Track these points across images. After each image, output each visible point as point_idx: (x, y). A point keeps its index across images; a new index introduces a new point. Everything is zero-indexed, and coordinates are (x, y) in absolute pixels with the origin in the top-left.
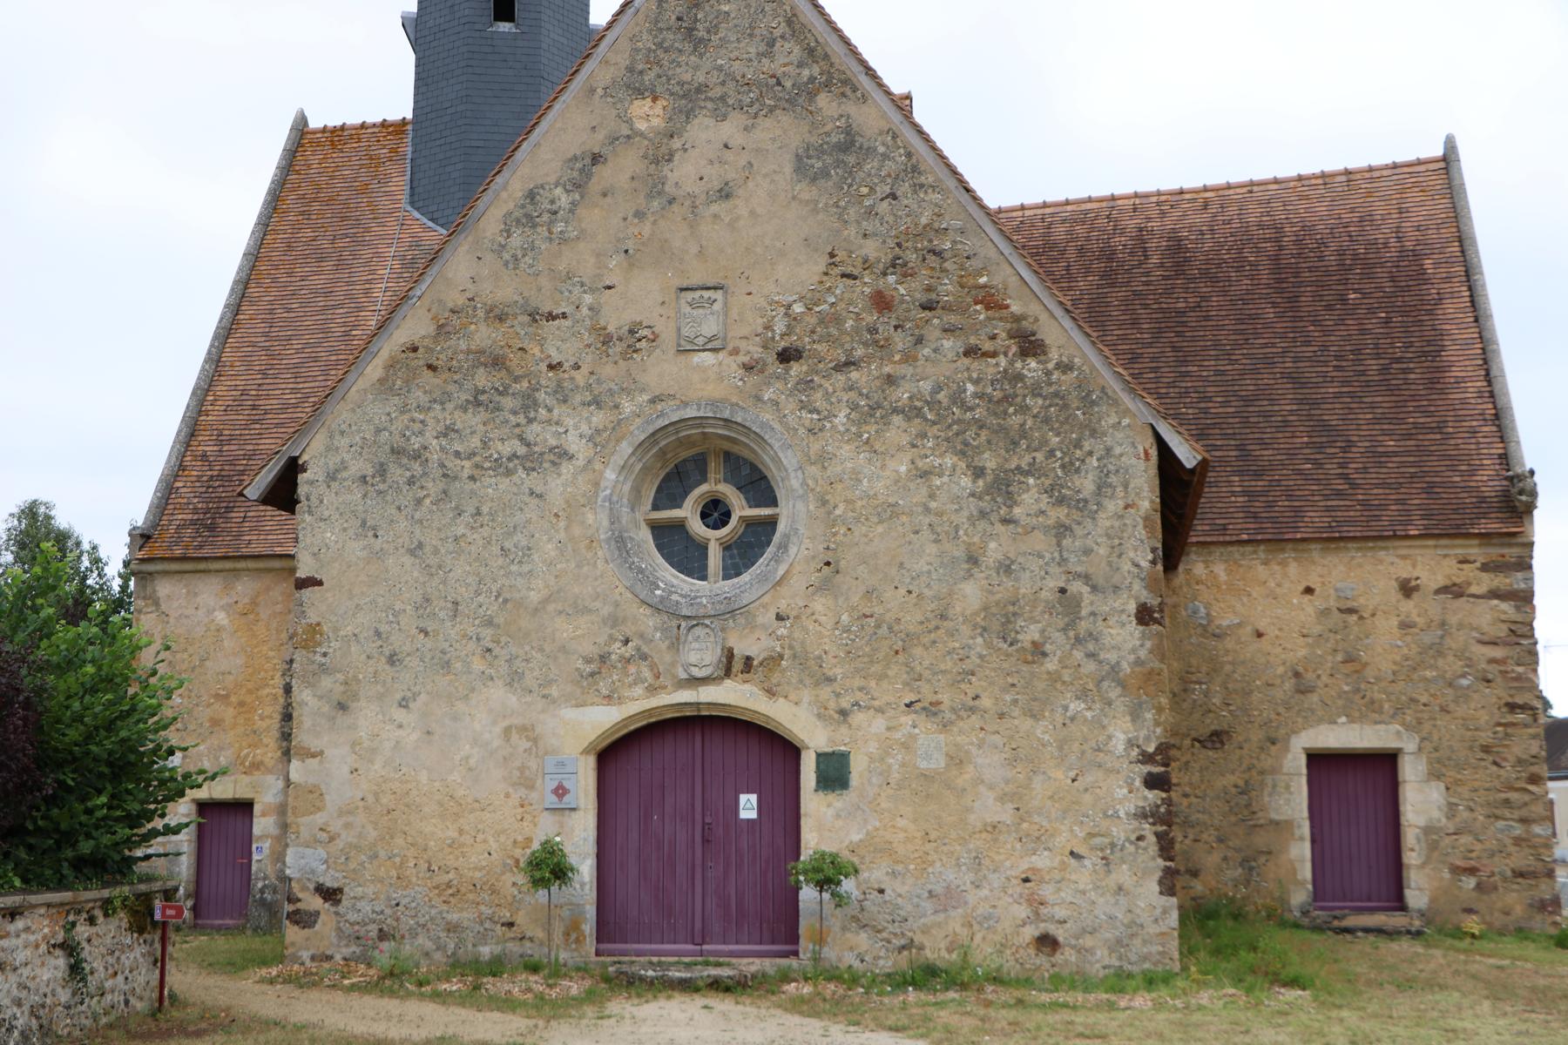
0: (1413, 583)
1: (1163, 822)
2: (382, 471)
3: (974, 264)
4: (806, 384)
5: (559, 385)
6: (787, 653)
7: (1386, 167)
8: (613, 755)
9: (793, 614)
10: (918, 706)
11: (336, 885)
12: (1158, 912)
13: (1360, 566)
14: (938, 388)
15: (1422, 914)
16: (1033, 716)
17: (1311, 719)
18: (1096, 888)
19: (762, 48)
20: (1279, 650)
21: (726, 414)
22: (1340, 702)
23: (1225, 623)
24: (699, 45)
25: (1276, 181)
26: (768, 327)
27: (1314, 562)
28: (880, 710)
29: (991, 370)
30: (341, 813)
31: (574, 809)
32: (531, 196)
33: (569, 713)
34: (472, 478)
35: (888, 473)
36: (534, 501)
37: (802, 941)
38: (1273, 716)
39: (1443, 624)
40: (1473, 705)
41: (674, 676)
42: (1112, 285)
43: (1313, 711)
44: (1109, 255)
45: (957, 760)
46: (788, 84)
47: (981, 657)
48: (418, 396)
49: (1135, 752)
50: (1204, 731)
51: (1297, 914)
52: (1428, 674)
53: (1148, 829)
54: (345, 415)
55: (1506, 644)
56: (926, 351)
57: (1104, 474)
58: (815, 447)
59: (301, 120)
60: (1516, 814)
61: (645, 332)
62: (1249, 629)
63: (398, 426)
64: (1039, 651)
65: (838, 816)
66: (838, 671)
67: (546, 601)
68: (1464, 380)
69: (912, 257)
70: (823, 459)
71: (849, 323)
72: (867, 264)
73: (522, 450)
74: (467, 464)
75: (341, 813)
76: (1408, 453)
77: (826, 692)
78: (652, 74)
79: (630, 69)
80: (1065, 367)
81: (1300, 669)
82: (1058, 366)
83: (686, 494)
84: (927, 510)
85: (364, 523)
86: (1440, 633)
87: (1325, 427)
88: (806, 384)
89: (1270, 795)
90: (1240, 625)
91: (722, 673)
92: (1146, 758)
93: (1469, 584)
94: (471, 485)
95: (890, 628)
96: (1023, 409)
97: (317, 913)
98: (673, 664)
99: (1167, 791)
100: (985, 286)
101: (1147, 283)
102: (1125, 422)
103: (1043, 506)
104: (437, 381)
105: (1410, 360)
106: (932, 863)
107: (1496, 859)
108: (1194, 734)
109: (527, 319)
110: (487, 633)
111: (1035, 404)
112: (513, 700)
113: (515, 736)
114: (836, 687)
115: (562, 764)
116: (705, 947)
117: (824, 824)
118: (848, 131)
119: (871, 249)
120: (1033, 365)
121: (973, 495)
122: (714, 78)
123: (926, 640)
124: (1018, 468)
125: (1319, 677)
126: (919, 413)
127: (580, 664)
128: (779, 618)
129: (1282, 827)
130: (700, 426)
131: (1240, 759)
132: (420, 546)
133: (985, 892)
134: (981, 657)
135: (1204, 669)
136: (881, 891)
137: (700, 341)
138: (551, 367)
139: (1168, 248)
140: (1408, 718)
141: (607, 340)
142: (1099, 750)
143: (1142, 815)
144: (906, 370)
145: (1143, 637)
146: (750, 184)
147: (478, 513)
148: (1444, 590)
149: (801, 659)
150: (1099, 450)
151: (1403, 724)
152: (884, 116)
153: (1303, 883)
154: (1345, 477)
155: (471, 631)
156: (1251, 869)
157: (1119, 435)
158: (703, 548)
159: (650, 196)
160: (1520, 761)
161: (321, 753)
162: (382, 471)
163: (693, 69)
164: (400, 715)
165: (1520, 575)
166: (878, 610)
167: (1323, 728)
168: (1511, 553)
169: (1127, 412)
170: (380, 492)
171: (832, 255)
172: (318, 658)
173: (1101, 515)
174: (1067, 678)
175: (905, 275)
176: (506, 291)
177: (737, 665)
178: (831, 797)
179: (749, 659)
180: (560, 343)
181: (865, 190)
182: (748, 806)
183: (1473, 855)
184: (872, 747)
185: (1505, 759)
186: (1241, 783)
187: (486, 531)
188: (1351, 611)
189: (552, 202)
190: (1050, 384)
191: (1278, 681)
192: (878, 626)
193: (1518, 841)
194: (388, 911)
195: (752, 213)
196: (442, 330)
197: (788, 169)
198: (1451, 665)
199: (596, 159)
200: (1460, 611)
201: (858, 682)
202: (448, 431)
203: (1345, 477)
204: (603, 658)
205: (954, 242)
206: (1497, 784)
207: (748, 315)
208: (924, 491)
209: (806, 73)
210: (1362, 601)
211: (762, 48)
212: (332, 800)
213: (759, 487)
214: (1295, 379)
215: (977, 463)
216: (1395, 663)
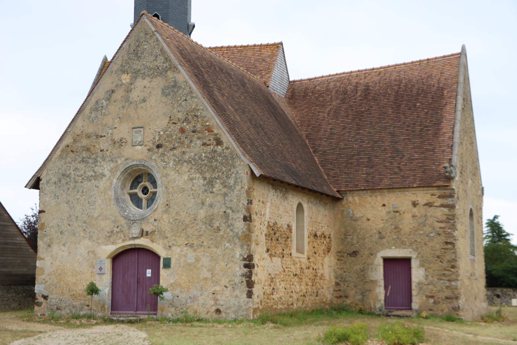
0: (417, 202)
1: (248, 278)
2: (60, 181)
3: (206, 119)
4: (163, 154)
5: (103, 156)
6: (157, 230)
7: (441, 57)
8: (117, 258)
9: (158, 219)
10: (188, 245)
12: (246, 303)
13: (400, 197)
14: (195, 155)
15: (416, 311)
16: (217, 247)
17: (383, 247)
18: (231, 296)
19: (154, 58)
20: (374, 225)
21: (143, 163)
22: (393, 242)
23: (358, 216)
24: (139, 58)
25: (404, 64)
26: (154, 138)
27: (385, 196)
28: (179, 246)
29: (209, 149)
30: (48, 275)
31: (104, 274)
32: (97, 102)
33: (103, 247)
34: (81, 182)
35: (182, 179)
36: (96, 188)
37: (158, 311)
38: (372, 246)
39: (426, 216)
40: (434, 243)
41: (129, 237)
42: (344, 103)
43: (384, 245)
44: (345, 92)
45: (197, 260)
46: (160, 68)
47: (204, 231)
48: (69, 159)
49: (242, 258)
50: (351, 251)
51: (378, 310)
52: (421, 232)
53: (244, 279)
54: (51, 165)
55: (445, 222)
56: (193, 144)
57: (236, 178)
58: (165, 172)
60: (447, 278)
61: (124, 140)
62: (365, 218)
63: (64, 168)
64: (218, 229)
65: (168, 276)
66: (169, 235)
67: (99, 216)
68: (446, 133)
69: (190, 117)
70: (167, 176)
71: (174, 137)
72: (179, 120)
73: (93, 174)
74: (80, 178)
75: (48, 275)
76: (421, 159)
77: (166, 241)
78: (127, 67)
79: (122, 65)
80: (227, 148)
81: (381, 231)
82: (226, 148)
84: (192, 189)
85: (55, 195)
86: (424, 219)
87: (397, 151)
88: (163, 154)
89: (371, 272)
90: (363, 217)
91: (140, 236)
92: (244, 259)
93: (434, 202)
94: (81, 184)
95: (182, 223)
96: (217, 160)
97: (42, 303)
98: (129, 233)
99: (250, 268)
100: (208, 125)
101: (354, 102)
102: (242, 164)
103: (221, 188)
104: (73, 155)
105: (430, 126)
106: (191, 289)
107: (440, 293)
108: (348, 252)
109: (95, 137)
110: (84, 225)
111: (219, 159)
112: (90, 244)
114: (168, 239)
115: (101, 261)
116: (137, 312)
117: (166, 278)
118: (175, 82)
119: (180, 115)
120: (220, 148)
121: (203, 185)
122: (142, 68)
123: (191, 226)
124: (215, 177)
125: (386, 233)
126: (190, 162)
127: (106, 233)
128: (155, 220)
130: (137, 166)
131: (362, 260)
132: (69, 201)
133: (203, 297)
134: (204, 231)
135: (351, 231)
137: (137, 143)
138: (101, 151)
139: (364, 89)
140: (414, 247)
142: (233, 257)
143: (243, 275)
144: (188, 150)
145: (244, 225)
146: (151, 98)
147: (83, 192)
148: (426, 204)
149: (160, 232)
150: (235, 172)
151: (412, 249)
152: (184, 77)
153: (380, 300)
154: (399, 167)
155: (80, 224)
156: (364, 296)
157: (240, 168)
158: (141, 200)
159: (126, 102)
160: (449, 261)
161: (44, 259)
162: (60, 181)
163: (137, 65)
164: (63, 248)
165: (450, 199)
166: (179, 218)
167: (387, 250)
168: (448, 192)
169: (242, 161)
170: (59, 186)
171: (170, 117)
172: (44, 232)
173: (235, 190)
174: (225, 237)
175: (188, 123)
176: (90, 129)
177: (144, 234)
179: (147, 232)
180: (104, 144)
181: (179, 99)
182: (149, 273)
183: (433, 292)
184: (177, 256)
185: (444, 260)
186: (362, 268)
187: (84, 197)
188: (397, 212)
189: (102, 104)
190: (223, 153)
191: (374, 235)
192: (179, 222)
193: (447, 287)
194: (59, 302)
195: (151, 106)
196: (75, 141)
197: (160, 93)
198: (428, 229)
199: (113, 91)
200: (431, 211)
201: (174, 238)
202: (76, 169)
203: (399, 167)
204: (112, 232)
205: (201, 113)
206: (441, 268)
207: (150, 135)
208: (191, 184)
209: (165, 65)
210: (400, 208)
211: (154, 58)
212: (47, 272)
213: (154, 183)
214: (392, 134)
215: (205, 176)
216: (410, 229)
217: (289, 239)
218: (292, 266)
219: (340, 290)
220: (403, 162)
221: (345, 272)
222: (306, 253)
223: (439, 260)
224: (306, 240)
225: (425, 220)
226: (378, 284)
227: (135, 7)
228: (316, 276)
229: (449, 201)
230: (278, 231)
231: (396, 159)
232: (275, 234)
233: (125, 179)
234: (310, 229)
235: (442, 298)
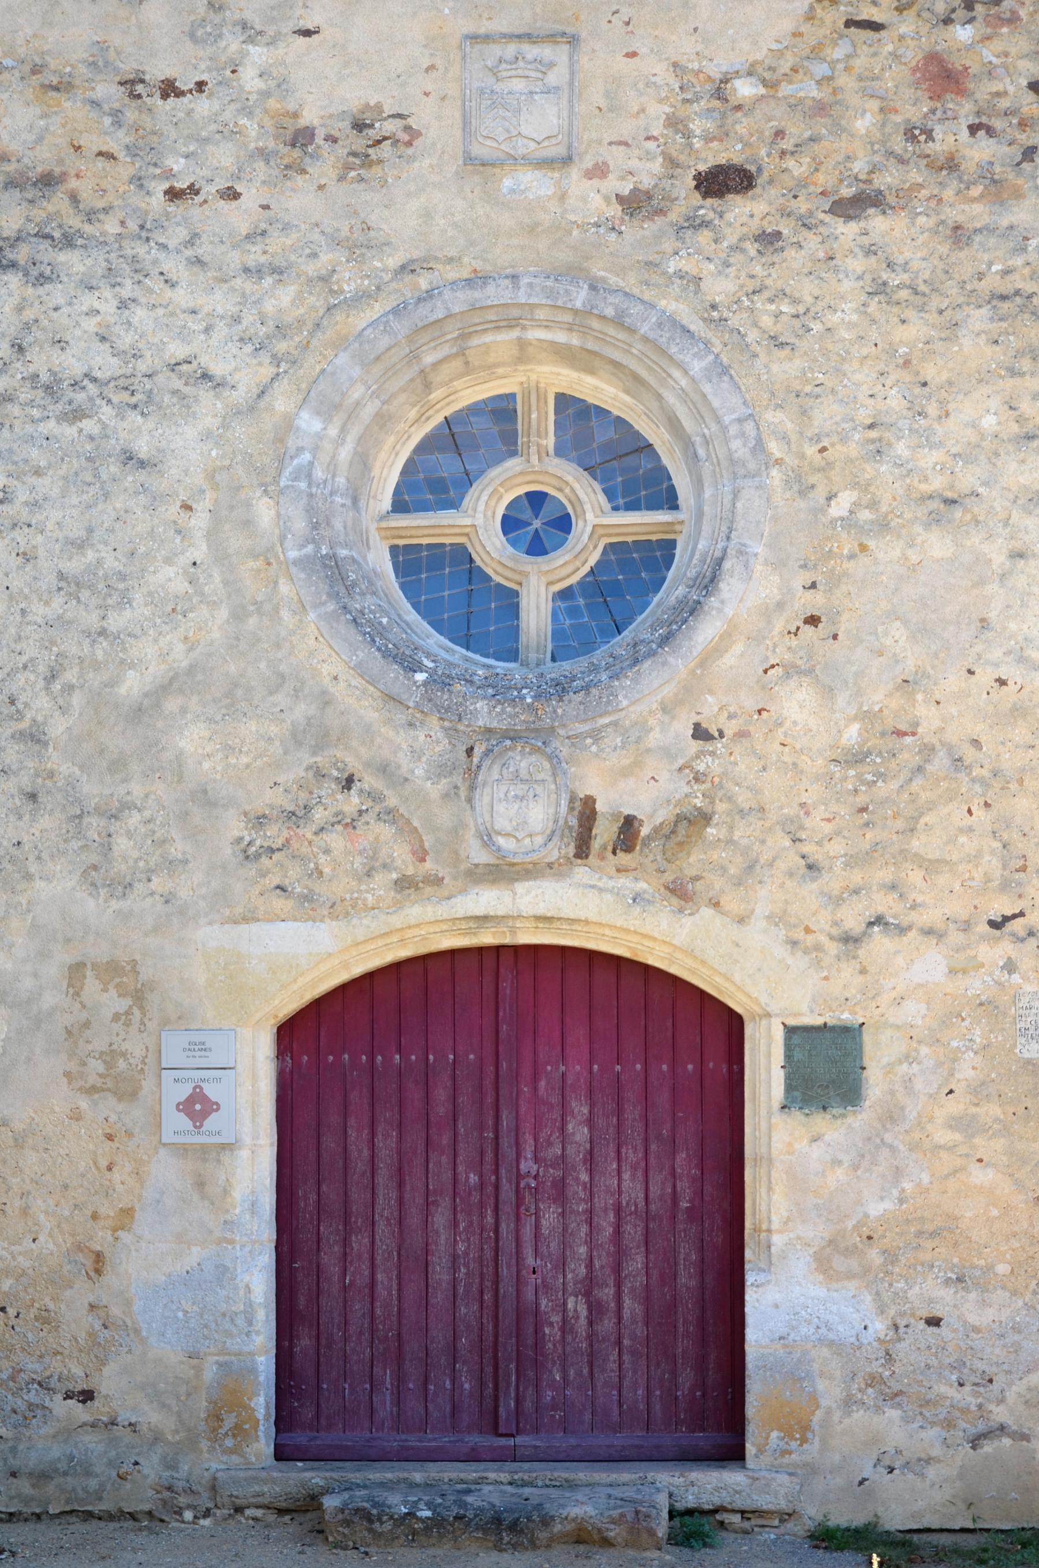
10: (1017, 926)
61: (390, 127)
98: (457, 830)
113: (91, 986)
128: (700, 733)
141: (302, 138)
158: (509, 601)
177: (604, 832)
178: (820, 1121)
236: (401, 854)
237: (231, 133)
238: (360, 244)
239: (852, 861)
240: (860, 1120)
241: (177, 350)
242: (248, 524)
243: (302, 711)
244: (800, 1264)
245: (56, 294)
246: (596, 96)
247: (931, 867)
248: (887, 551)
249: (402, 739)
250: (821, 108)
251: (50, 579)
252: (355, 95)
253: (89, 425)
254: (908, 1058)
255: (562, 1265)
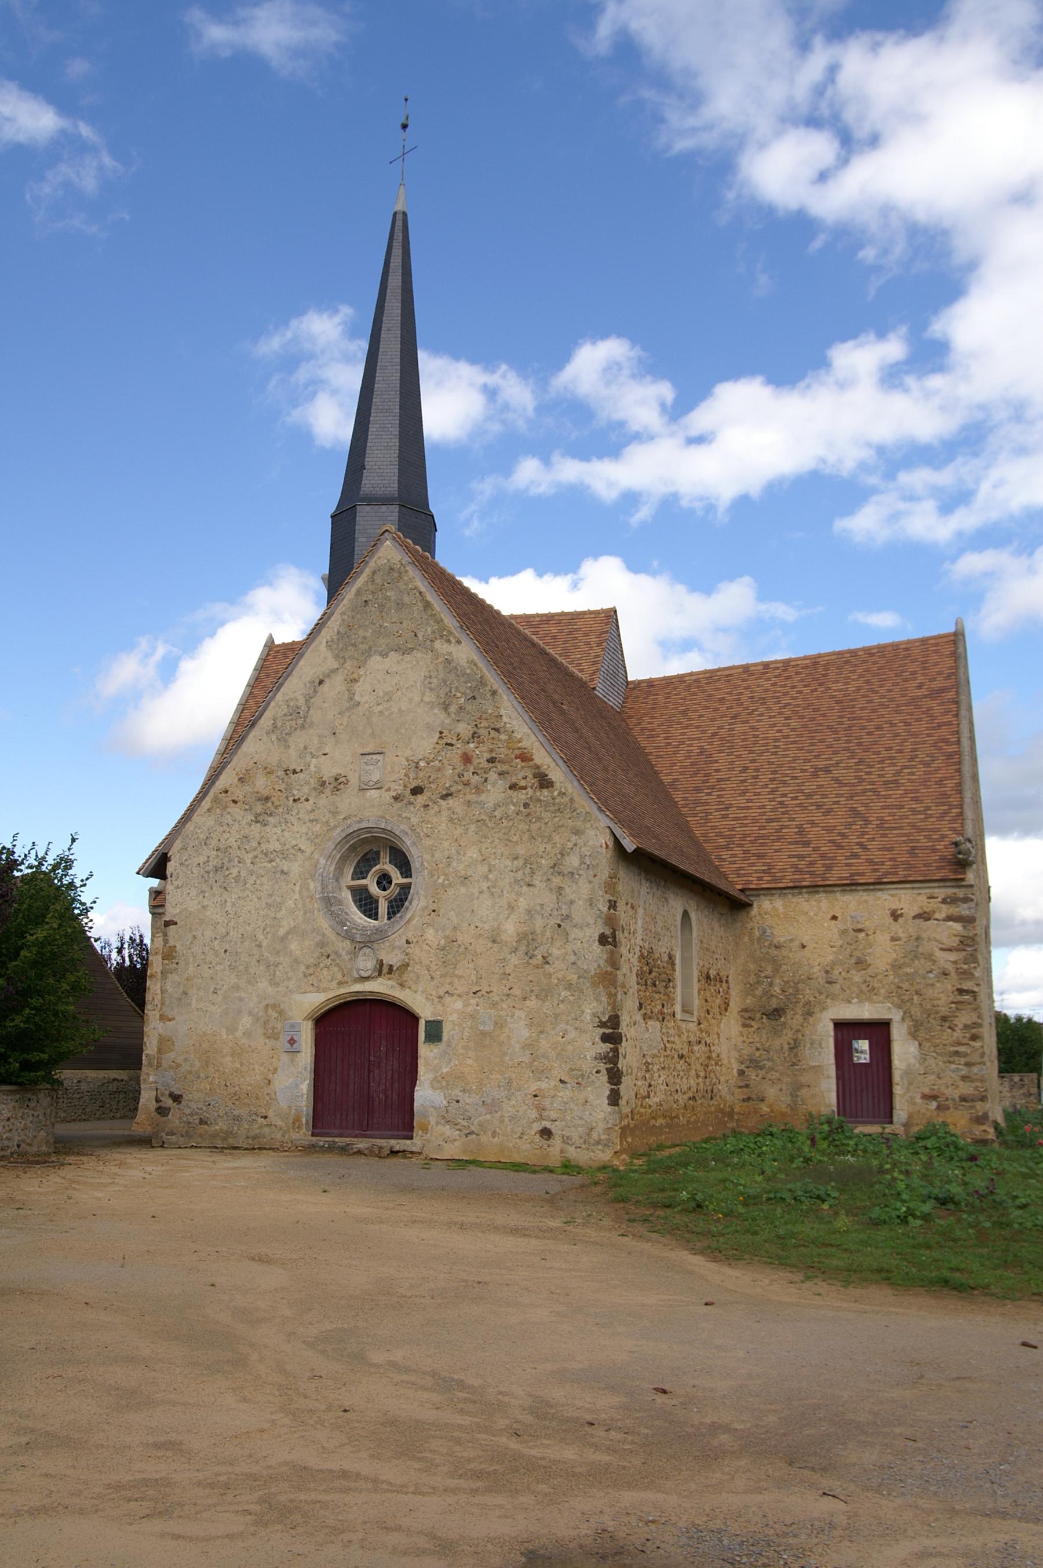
0: (899, 912)
11: (179, 1093)
27: (837, 900)
33: (298, 997)
53: (602, 1067)
55: (957, 950)
59: (270, 641)
60: (963, 1060)
61: (342, 780)
62: (797, 943)
83: (368, 872)
90: (791, 940)
92: (602, 1025)
93: (934, 912)
98: (351, 969)
113: (270, 1010)
128: (408, 942)
129: (818, 1069)
130: (370, 832)
136: (458, 1102)
137: (371, 783)
141: (323, 784)
160: (966, 1027)
165: (965, 906)
171: (441, 733)
177: (385, 970)
178: (432, 1046)
188: (860, 930)
193: (964, 1078)
194: (204, 1108)
210: (867, 924)
217: (671, 984)
218: (676, 1039)
219: (747, 1086)
220: (867, 833)
221: (758, 1049)
222: (695, 1013)
223: (947, 1024)
224: (696, 986)
225: (917, 947)
226: (826, 1073)
227: (332, 545)
228: (709, 1058)
229: (964, 910)
230: (654, 966)
231: (854, 827)
232: (650, 972)
233: (344, 859)
234: (701, 964)
235: (953, 1100)
236: (339, 976)
237: (307, 783)
238: (335, 813)
239: (442, 976)
240: (442, 1045)
241: (294, 843)
242: (308, 889)
243: (319, 938)
244: (427, 1085)
245: (268, 829)
246: (389, 769)
247: (460, 977)
248: (451, 892)
249: (340, 945)
250: (439, 770)
251: (264, 905)
252: (336, 771)
253: (274, 864)
254: (453, 1029)
255: (379, 1085)
